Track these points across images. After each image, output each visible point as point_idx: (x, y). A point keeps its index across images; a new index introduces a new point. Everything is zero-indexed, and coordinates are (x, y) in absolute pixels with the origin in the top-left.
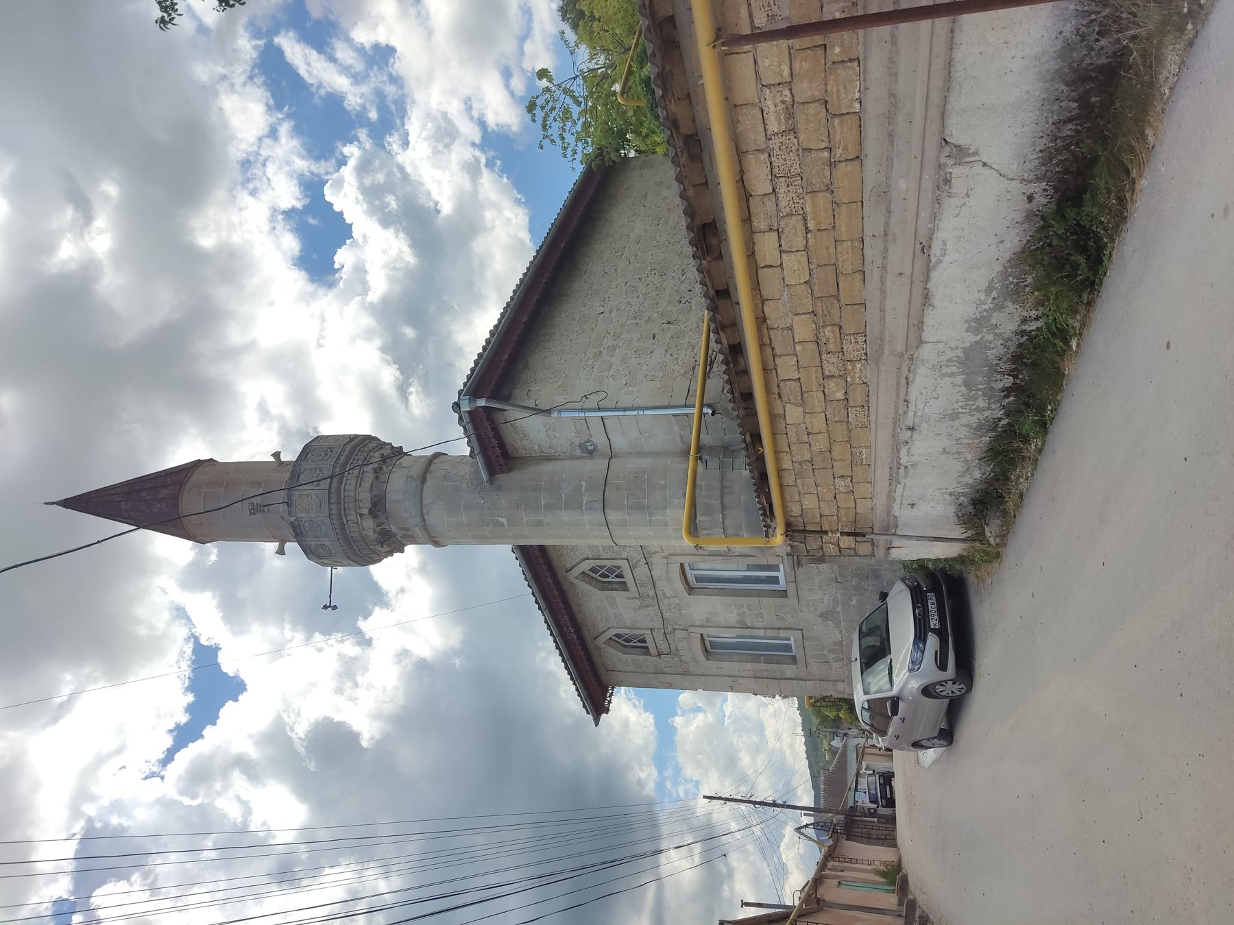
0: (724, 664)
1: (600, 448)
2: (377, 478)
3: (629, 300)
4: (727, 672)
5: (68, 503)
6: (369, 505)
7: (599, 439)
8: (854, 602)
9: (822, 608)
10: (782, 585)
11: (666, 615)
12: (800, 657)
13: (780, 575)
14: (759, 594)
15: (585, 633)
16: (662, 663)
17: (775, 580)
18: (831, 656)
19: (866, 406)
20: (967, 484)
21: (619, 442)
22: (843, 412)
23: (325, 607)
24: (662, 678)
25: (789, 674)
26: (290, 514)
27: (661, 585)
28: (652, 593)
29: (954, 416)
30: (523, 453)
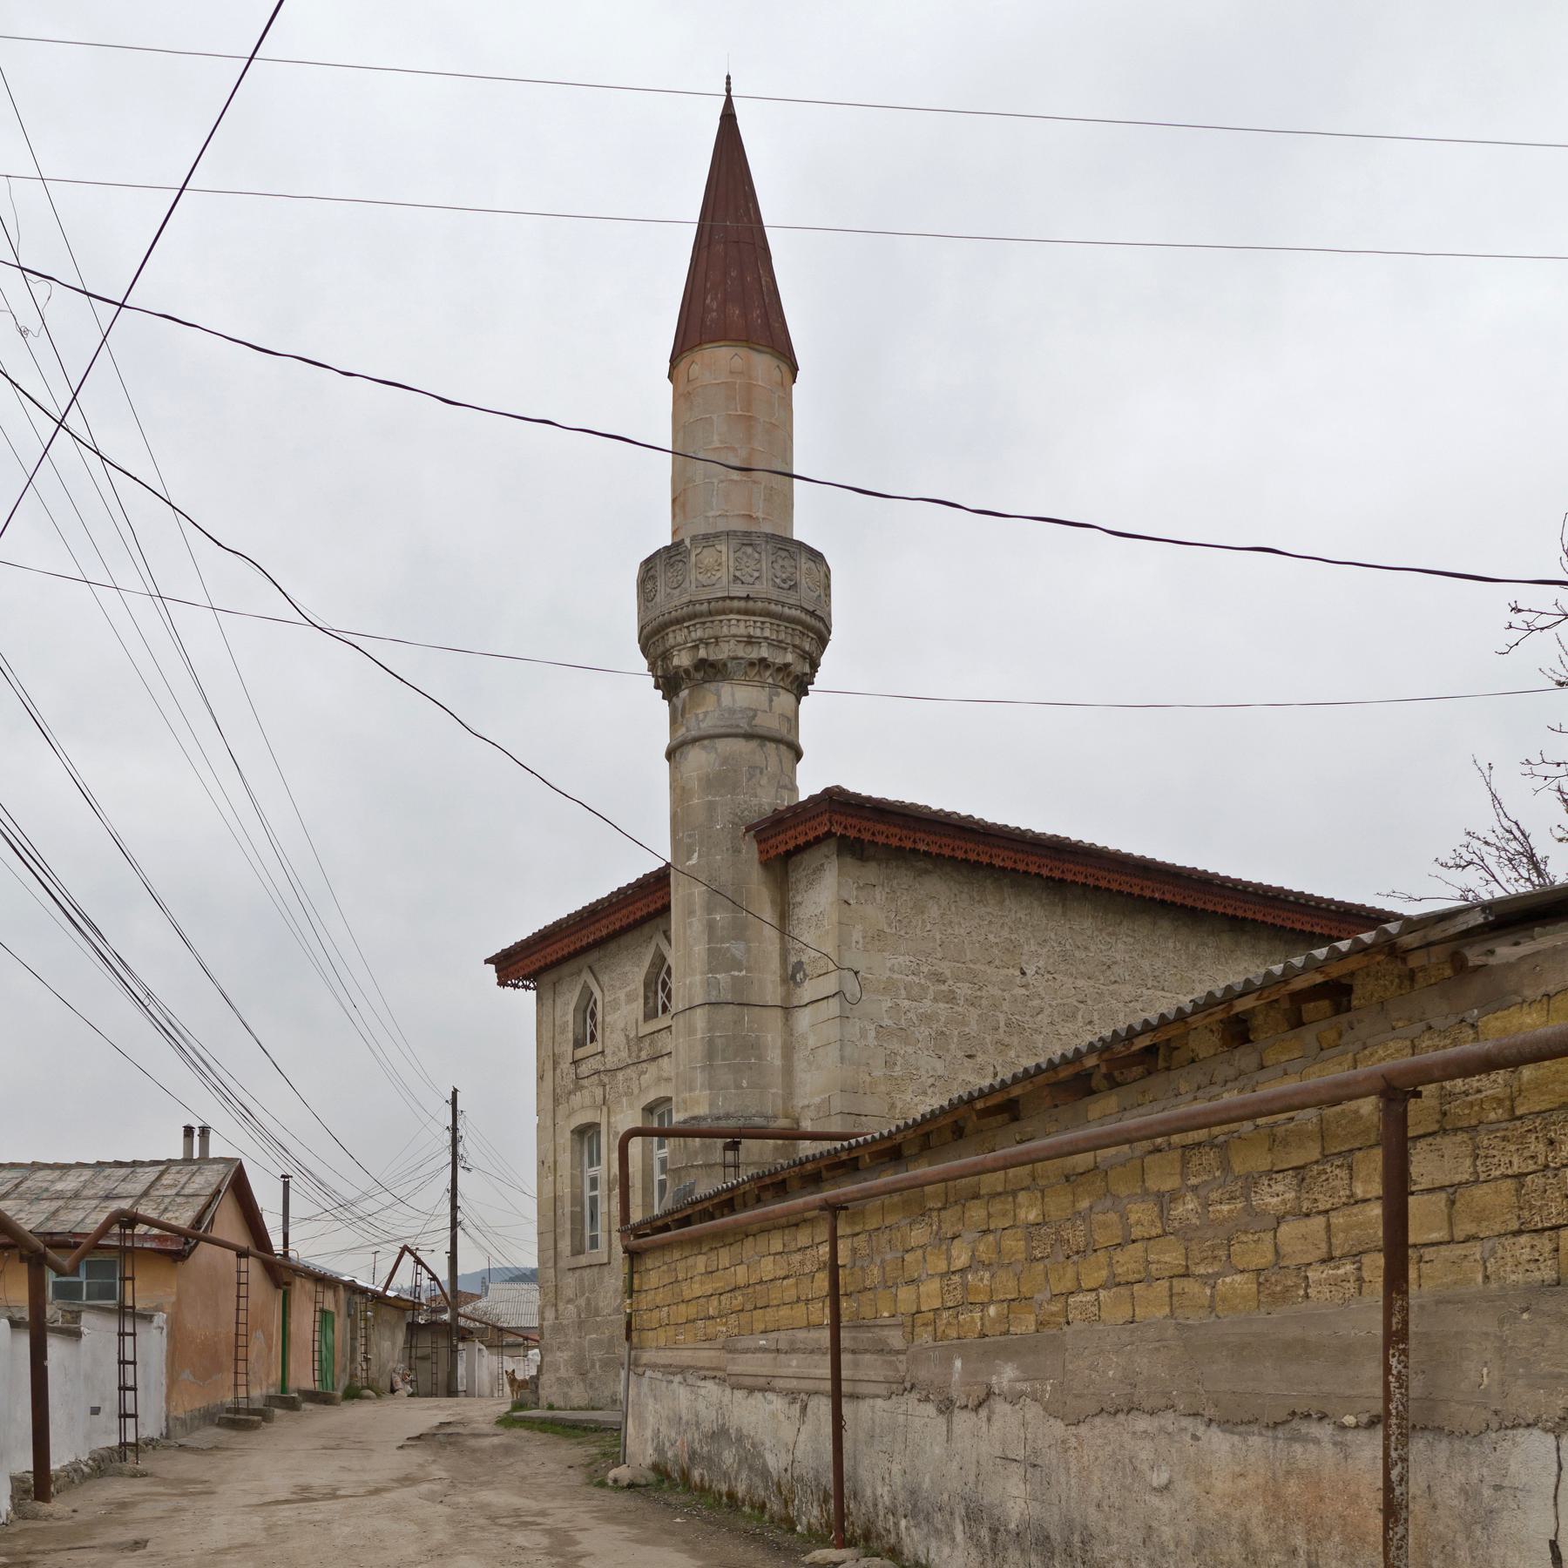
0: (568, 1154)
2: (752, 664)
3: (1048, 1011)
4: (559, 1159)
5: (728, 119)
7: (808, 991)
11: (620, 1075)
12: (583, 1260)
18: (582, 1302)
24: (549, 1065)
26: (694, 538)
27: (652, 1069)
30: (793, 877)
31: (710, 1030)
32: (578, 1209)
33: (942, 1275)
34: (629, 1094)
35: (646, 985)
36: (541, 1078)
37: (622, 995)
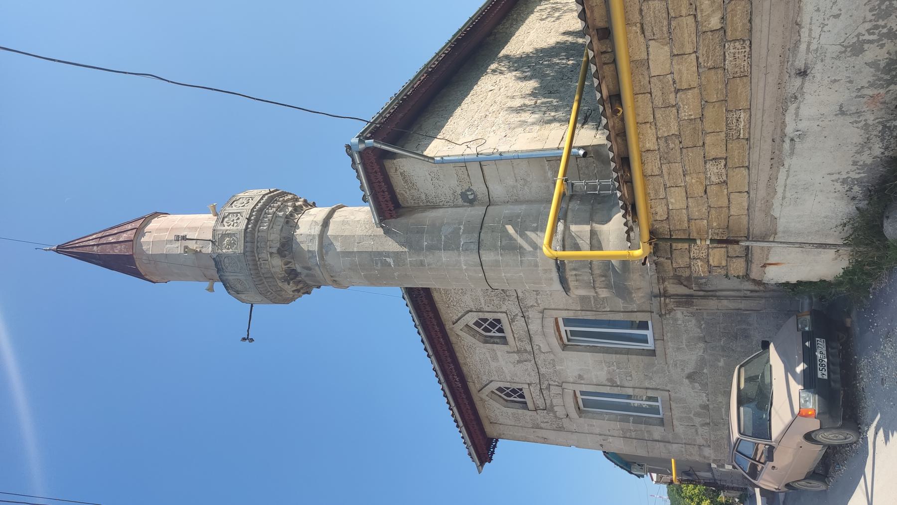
0: (594, 422)
1: (480, 196)
2: (287, 222)
6: (278, 245)
7: (479, 188)
8: (721, 364)
9: (689, 369)
10: (650, 346)
11: (543, 370)
13: (649, 333)
14: (628, 352)
15: (471, 385)
16: (540, 417)
17: (645, 340)
18: (698, 421)
19: (748, 40)
20: (865, 165)
21: (498, 191)
22: (719, 51)
23: (244, 339)
25: (656, 436)
27: (538, 340)
28: (529, 348)
29: (857, 49)
30: (411, 203)
31: (496, 249)
32: (631, 419)
33: (724, 41)
34: (553, 363)
35: (486, 342)
36: (545, 441)
37: (494, 365)
